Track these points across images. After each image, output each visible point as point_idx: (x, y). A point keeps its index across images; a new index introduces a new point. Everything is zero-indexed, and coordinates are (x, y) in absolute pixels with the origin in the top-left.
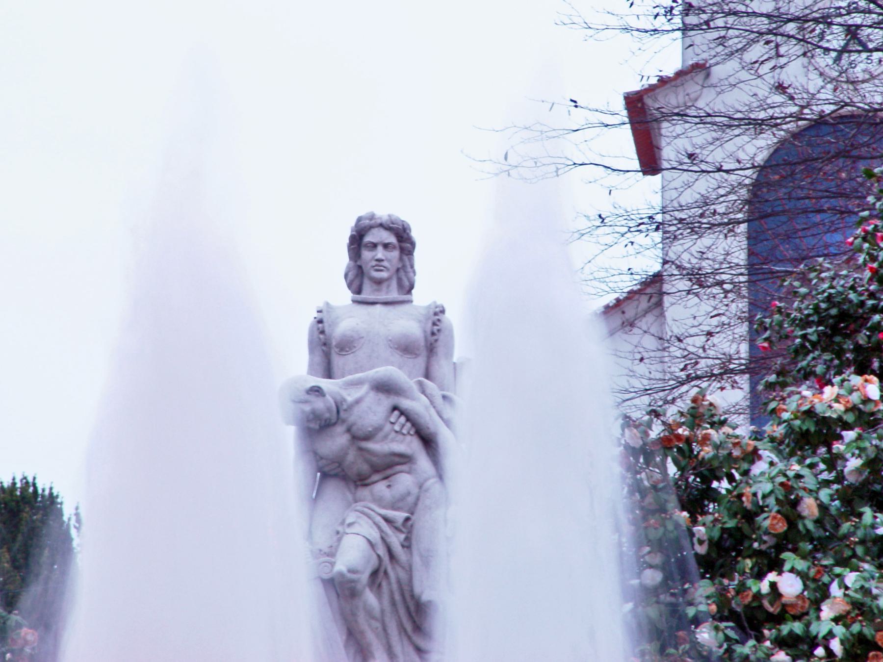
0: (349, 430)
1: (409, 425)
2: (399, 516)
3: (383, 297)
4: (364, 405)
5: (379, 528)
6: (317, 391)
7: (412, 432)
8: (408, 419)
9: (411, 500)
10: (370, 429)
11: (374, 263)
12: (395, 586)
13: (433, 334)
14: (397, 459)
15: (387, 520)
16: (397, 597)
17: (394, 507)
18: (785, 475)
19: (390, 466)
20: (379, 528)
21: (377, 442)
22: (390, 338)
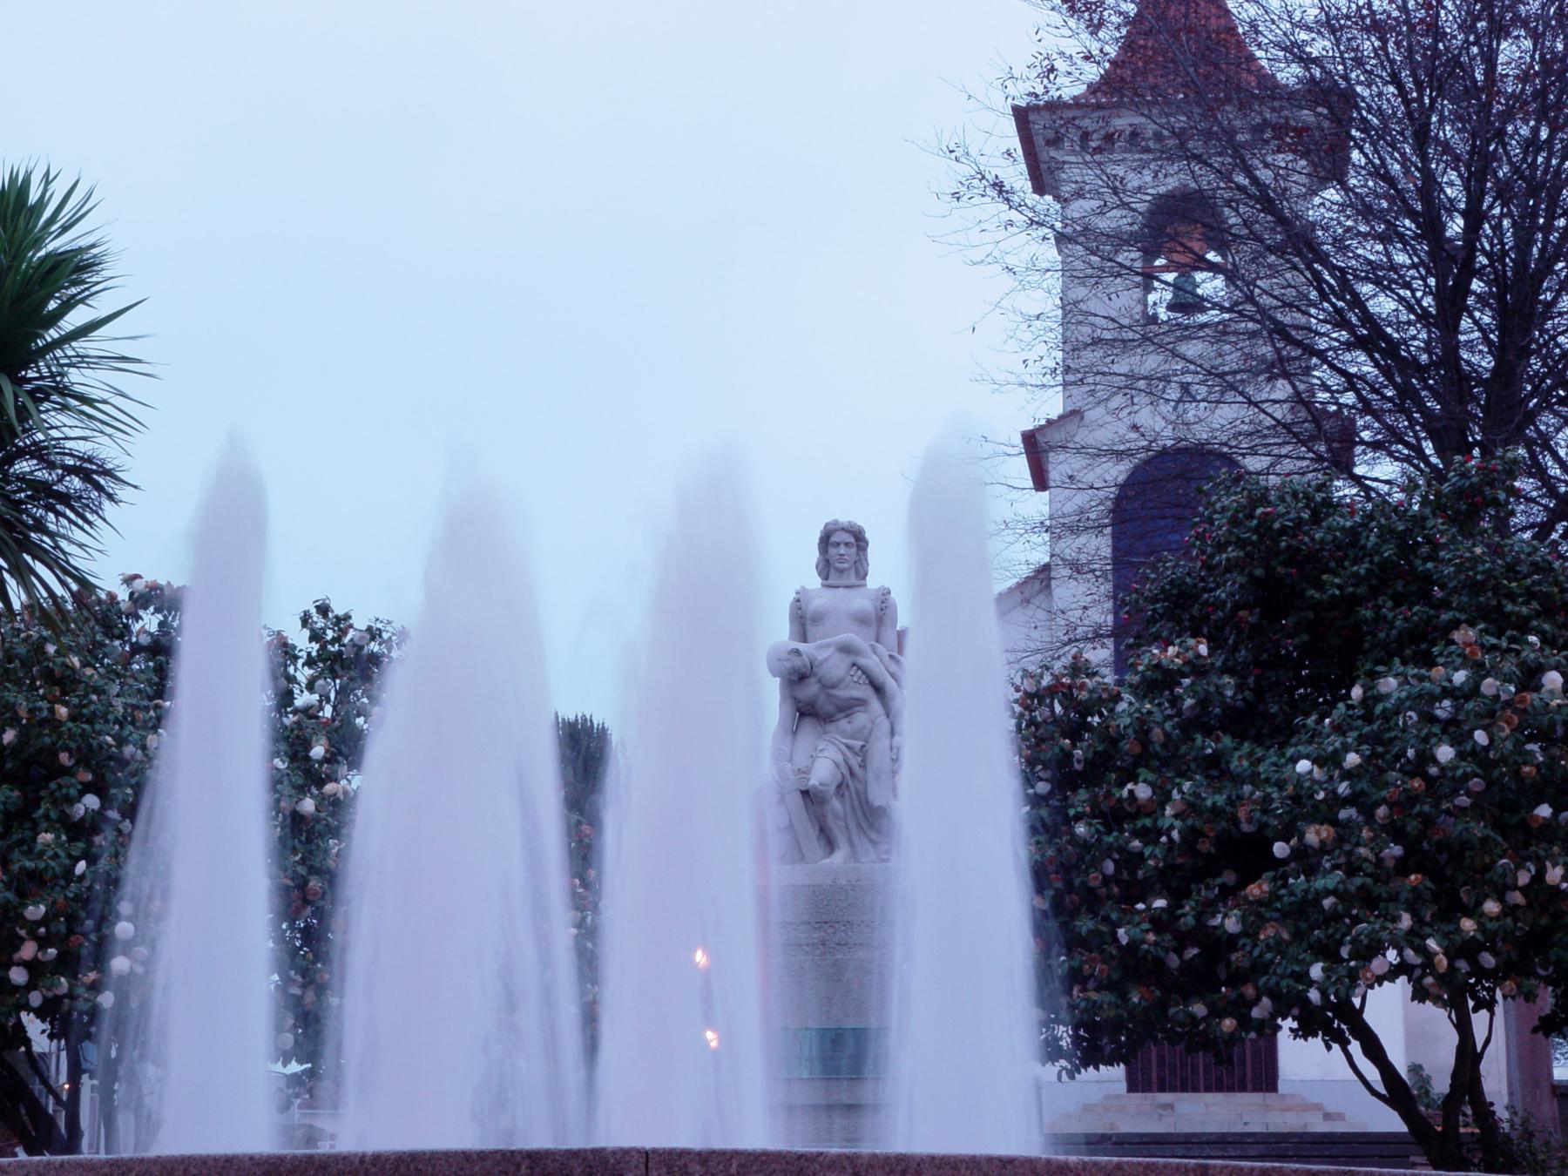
0: (819, 681)
2: (857, 744)
8: (864, 673)
9: (866, 732)
15: (848, 747)
16: (856, 803)
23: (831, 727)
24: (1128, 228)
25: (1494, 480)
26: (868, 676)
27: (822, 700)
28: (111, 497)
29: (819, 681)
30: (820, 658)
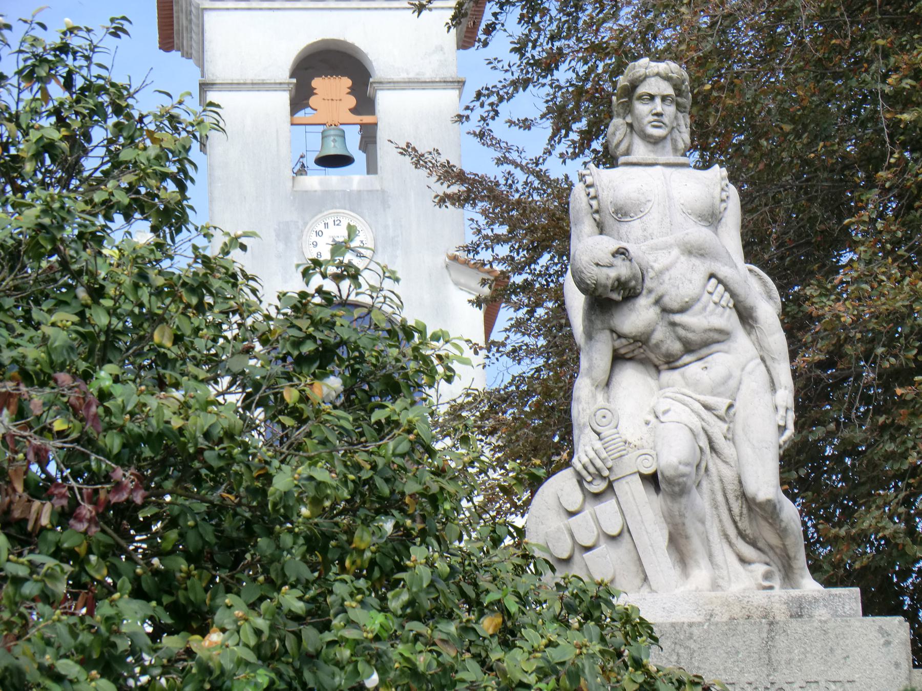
0: (657, 302)
1: (727, 295)
2: (721, 403)
3: (662, 159)
4: (673, 272)
5: (699, 416)
6: (623, 254)
7: (731, 305)
8: (727, 289)
9: (733, 383)
10: (687, 300)
11: (651, 118)
12: (717, 486)
13: (723, 201)
14: (716, 336)
15: (707, 407)
16: (720, 498)
17: (714, 393)
18: (34, 654)
19: (706, 344)
20: (699, 416)
21: (695, 315)
22: (682, 202)
23: (667, 376)
24: (603, 35)
25: (774, 197)
26: (733, 295)
27: (660, 334)
28: (711, 556)
29: (657, 302)
30: (657, 266)
